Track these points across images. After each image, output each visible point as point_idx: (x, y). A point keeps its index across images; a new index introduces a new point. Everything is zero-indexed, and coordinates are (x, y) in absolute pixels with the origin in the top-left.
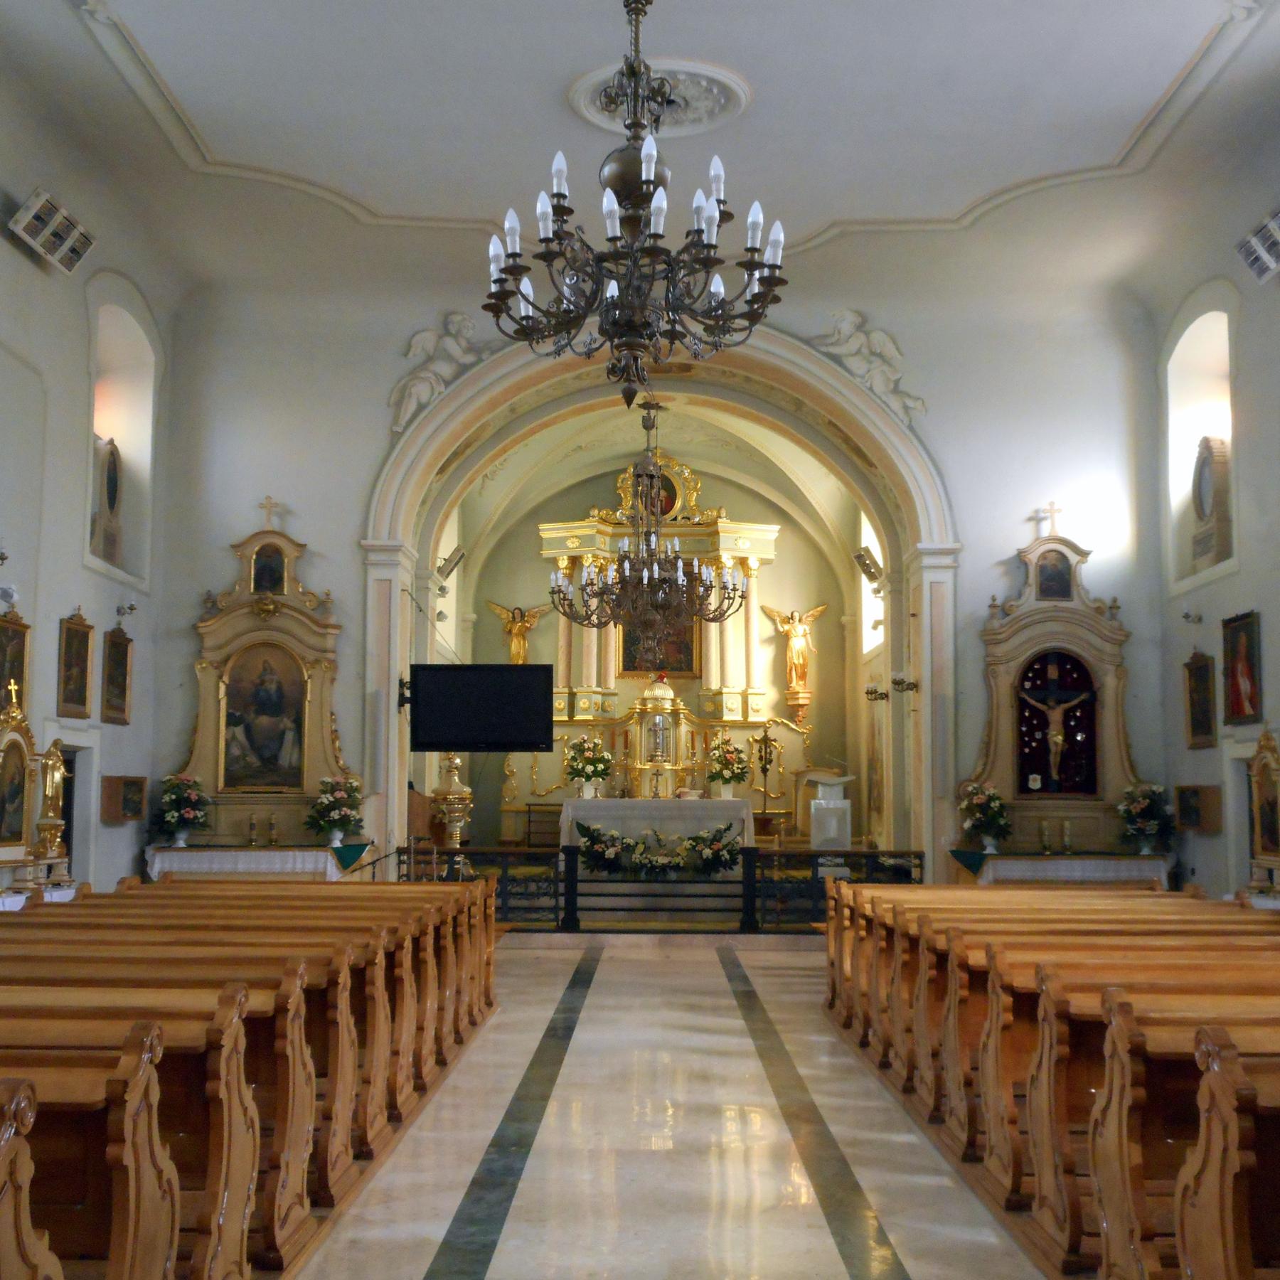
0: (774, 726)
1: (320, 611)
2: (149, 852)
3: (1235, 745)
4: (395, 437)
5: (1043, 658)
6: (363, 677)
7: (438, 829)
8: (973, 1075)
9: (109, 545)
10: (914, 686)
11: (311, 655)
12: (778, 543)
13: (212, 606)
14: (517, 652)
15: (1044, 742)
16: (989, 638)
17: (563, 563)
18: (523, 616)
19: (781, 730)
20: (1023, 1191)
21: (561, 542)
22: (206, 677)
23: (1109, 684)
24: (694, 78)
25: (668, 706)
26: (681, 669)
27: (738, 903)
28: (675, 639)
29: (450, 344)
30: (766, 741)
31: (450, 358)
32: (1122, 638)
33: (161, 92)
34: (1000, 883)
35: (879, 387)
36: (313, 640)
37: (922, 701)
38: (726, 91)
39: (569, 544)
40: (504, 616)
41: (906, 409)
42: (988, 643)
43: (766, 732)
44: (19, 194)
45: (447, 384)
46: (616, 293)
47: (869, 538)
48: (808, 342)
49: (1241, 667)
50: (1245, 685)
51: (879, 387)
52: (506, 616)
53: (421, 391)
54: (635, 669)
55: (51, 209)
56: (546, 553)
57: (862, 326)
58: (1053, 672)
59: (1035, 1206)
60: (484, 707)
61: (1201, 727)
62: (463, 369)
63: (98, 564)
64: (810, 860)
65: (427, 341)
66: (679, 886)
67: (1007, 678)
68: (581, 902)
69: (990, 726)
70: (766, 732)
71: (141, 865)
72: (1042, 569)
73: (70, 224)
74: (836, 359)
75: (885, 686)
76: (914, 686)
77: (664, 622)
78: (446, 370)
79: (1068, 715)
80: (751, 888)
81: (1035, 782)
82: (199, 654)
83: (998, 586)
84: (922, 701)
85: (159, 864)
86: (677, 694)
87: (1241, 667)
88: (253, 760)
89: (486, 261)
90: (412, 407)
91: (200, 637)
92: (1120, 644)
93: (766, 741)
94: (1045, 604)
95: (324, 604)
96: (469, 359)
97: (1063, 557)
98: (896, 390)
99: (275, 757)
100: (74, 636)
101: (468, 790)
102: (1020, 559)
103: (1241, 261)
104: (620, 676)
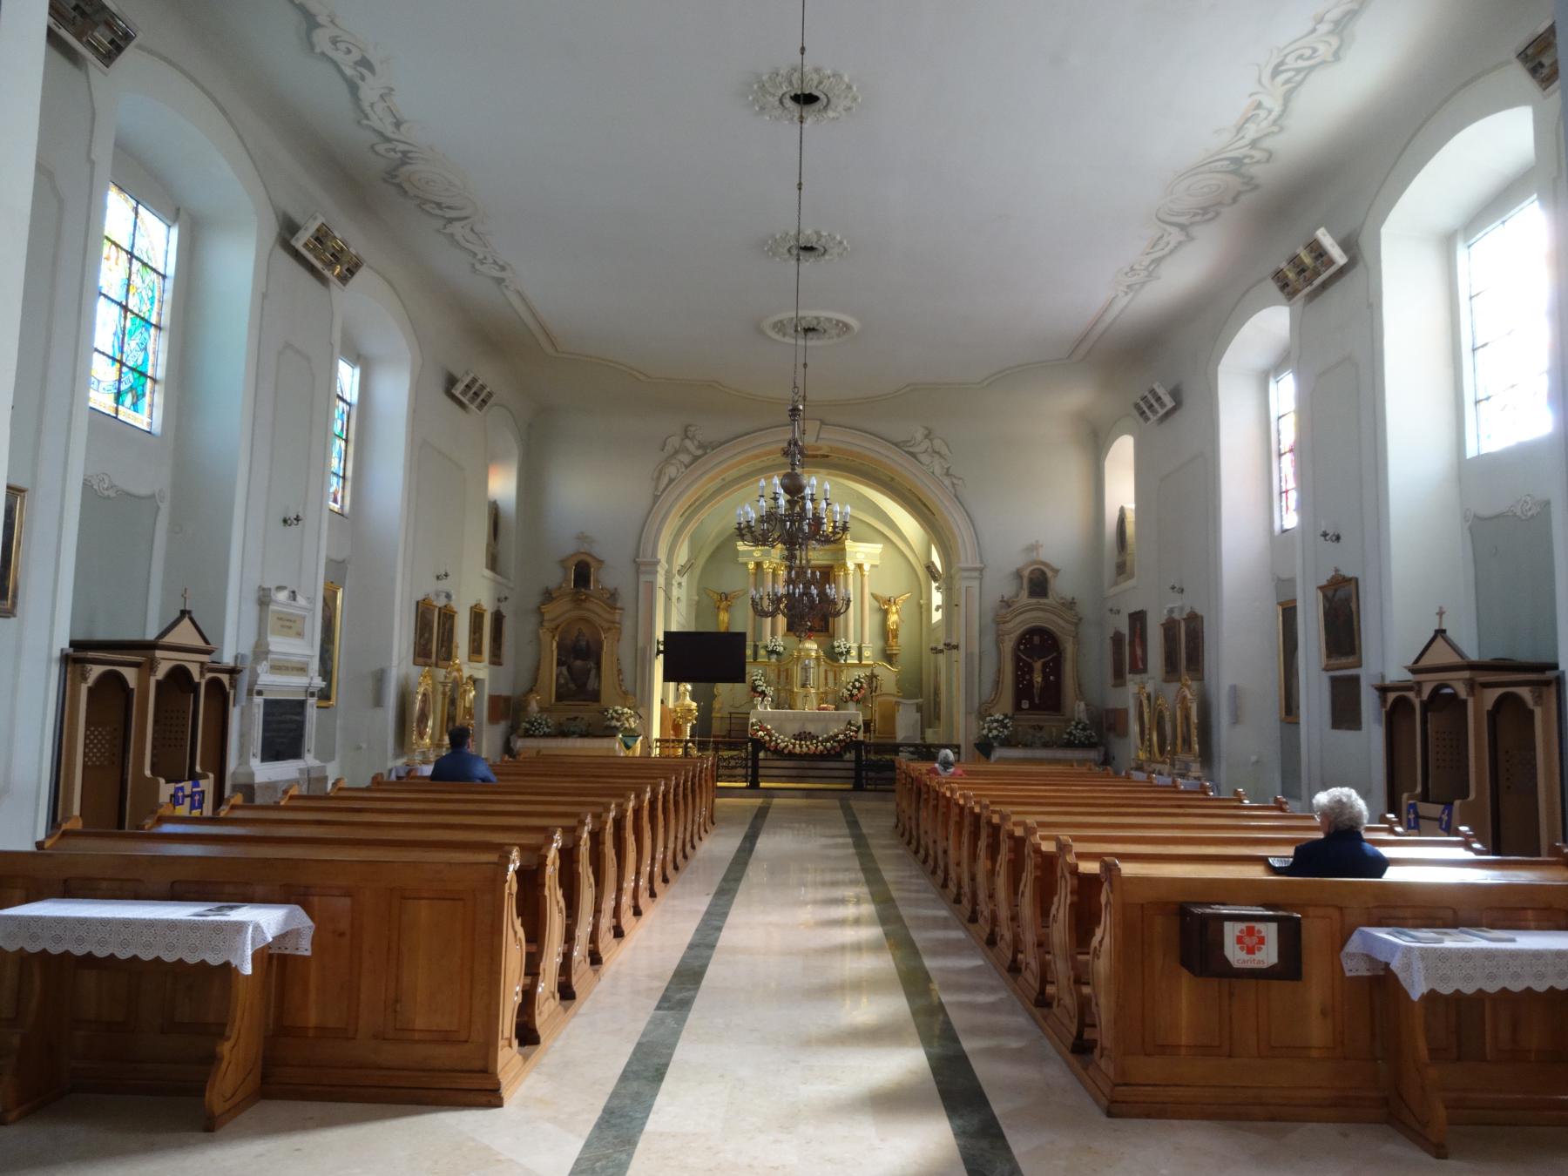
1: (611, 599)
2: (513, 738)
3: (1132, 685)
4: (656, 498)
5: (1032, 631)
6: (636, 638)
7: (677, 728)
9: (493, 563)
10: (956, 647)
11: (606, 625)
12: (882, 556)
13: (548, 596)
14: (724, 621)
15: (1031, 681)
16: (999, 621)
17: (751, 566)
20: (1086, 1036)
21: (750, 554)
22: (546, 637)
23: (1069, 648)
24: (829, 320)
27: (852, 774)
29: (688, 443)
30: (873, 677)
31: (687, 451)
32: (1078, 622)
33: (534, 315)
34: (1001, 760)
35: (938, 471)
36: (607, 616)
37: (960, 655)
38: (847, 326)
41: (953, 485)
42: (998, 623)
44: (458, 373)
45: (686, 467)
47: (936, 559)
48: (896, 445)
49: (1137, 641)
50: (1139, 652)
51: (938, 471)
52: (716, 597)
53: (671, 471)
55: (474, 380)
56: (741, 560)
57: (929, 435)
58: (1036, 639)
59: (1097, 1052)
60: (704, 657)
61: (1119, 675)
62: (696, 458)
63: (488, 573)
64: (895, 749)
65: (675, 442)
67: (1008, 646)
68: (761, 772)
69: (999, 671)
71: (508, 749)
72: (1031, 580)
73: (483, 387)
74: (913, 455)
75: (941, 647)
76: (956, 647)
77: (813, 611)
78: (686, 458)
79: (1045, 665)
80: (859, 764)
81: (1025, 704)
82: (541, 623)
83: (1008, 590)
84: (960, 655)
85: (519, 744)
87: (1137, 641)
88: (572, 686)
90: (665, 480)
91: (542, 614)
92: (1076, 625)
93: (873, 677)
94: (1034, 601)
95: (614, 595)
96: (699, 452)
97: (1043, 573)
98: (947, 474)
99: (585, 685)
100: (477, 616)
101: (694, 705)
102: (1018, 574)
103: (1135, 413)
104: (784, 635)
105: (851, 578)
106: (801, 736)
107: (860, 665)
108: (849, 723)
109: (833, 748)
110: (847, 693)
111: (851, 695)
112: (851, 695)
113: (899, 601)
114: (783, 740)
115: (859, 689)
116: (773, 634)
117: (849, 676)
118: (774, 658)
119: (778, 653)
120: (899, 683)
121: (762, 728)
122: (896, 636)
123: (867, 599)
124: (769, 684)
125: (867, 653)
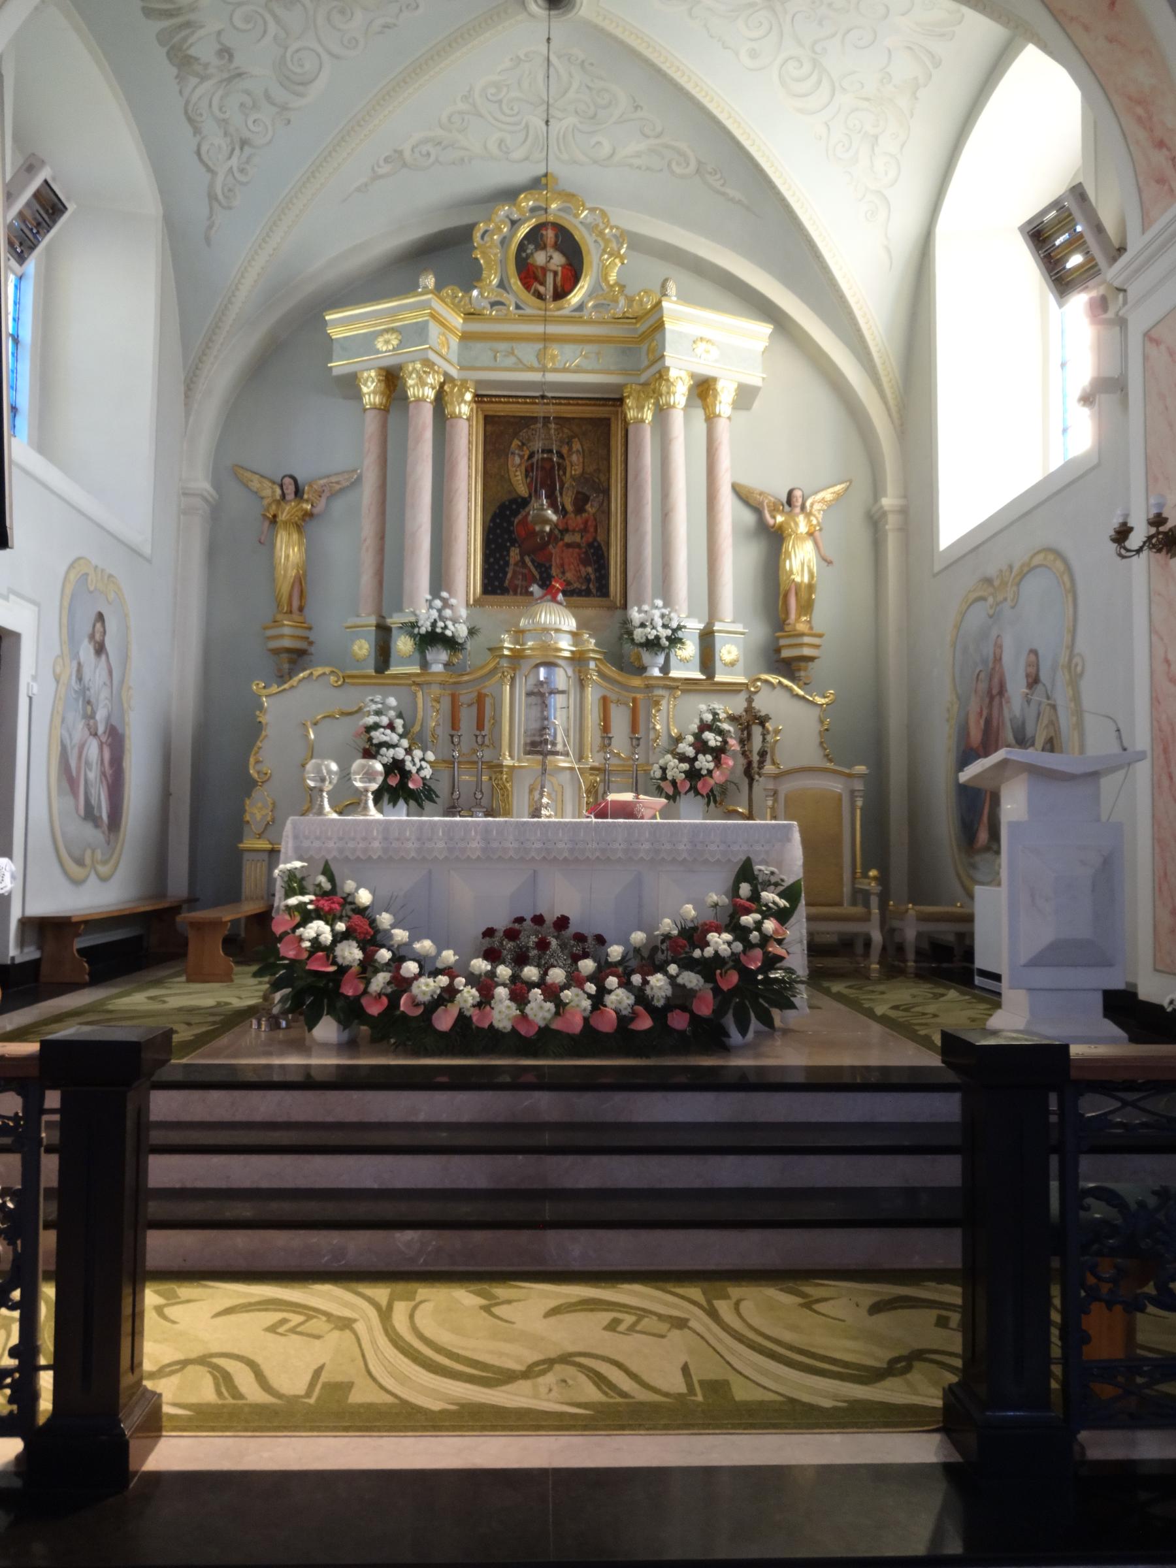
0: (765, 690)
8: (494, 249)
17: (370, 390)
18: (298, 492)
19: (780, 696)
21: (366, 343)
25: (565, 645)
26: (587, 593)
28: (576, 538)
30: (751, 721)
39: (380, 345)
40: (267, 492)
43: (750, 701)
46: (451, 952)
52: (271, 492)
54: (504, 591)
56: (338, 365)
66: (619, 1098)
70: (750, 701)
86: (581, 625)
89: (1048, 1112)
93: (751, 721)
105: (677, 419)
106: (521, 941)
107: (708, 684)
108: (746, 872)
109: (681, 997)
110: (676, 769)
111: (693, 775)
112: (693, 775)
113: (818, 502)
114: (434, 964)
115: (718, 753)
116: (440, 581)
117: (676, 718)
118: (438, 658)
119: (451, 644)
120: (826, 737)
121: (332, 904)
122: (807, 607)
123: (728, 508)
124: (416, 739)
125: (727, 651)
